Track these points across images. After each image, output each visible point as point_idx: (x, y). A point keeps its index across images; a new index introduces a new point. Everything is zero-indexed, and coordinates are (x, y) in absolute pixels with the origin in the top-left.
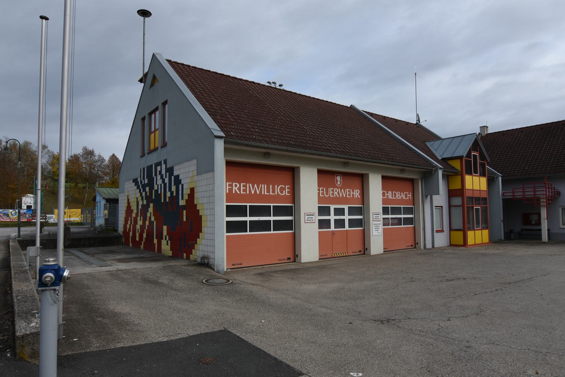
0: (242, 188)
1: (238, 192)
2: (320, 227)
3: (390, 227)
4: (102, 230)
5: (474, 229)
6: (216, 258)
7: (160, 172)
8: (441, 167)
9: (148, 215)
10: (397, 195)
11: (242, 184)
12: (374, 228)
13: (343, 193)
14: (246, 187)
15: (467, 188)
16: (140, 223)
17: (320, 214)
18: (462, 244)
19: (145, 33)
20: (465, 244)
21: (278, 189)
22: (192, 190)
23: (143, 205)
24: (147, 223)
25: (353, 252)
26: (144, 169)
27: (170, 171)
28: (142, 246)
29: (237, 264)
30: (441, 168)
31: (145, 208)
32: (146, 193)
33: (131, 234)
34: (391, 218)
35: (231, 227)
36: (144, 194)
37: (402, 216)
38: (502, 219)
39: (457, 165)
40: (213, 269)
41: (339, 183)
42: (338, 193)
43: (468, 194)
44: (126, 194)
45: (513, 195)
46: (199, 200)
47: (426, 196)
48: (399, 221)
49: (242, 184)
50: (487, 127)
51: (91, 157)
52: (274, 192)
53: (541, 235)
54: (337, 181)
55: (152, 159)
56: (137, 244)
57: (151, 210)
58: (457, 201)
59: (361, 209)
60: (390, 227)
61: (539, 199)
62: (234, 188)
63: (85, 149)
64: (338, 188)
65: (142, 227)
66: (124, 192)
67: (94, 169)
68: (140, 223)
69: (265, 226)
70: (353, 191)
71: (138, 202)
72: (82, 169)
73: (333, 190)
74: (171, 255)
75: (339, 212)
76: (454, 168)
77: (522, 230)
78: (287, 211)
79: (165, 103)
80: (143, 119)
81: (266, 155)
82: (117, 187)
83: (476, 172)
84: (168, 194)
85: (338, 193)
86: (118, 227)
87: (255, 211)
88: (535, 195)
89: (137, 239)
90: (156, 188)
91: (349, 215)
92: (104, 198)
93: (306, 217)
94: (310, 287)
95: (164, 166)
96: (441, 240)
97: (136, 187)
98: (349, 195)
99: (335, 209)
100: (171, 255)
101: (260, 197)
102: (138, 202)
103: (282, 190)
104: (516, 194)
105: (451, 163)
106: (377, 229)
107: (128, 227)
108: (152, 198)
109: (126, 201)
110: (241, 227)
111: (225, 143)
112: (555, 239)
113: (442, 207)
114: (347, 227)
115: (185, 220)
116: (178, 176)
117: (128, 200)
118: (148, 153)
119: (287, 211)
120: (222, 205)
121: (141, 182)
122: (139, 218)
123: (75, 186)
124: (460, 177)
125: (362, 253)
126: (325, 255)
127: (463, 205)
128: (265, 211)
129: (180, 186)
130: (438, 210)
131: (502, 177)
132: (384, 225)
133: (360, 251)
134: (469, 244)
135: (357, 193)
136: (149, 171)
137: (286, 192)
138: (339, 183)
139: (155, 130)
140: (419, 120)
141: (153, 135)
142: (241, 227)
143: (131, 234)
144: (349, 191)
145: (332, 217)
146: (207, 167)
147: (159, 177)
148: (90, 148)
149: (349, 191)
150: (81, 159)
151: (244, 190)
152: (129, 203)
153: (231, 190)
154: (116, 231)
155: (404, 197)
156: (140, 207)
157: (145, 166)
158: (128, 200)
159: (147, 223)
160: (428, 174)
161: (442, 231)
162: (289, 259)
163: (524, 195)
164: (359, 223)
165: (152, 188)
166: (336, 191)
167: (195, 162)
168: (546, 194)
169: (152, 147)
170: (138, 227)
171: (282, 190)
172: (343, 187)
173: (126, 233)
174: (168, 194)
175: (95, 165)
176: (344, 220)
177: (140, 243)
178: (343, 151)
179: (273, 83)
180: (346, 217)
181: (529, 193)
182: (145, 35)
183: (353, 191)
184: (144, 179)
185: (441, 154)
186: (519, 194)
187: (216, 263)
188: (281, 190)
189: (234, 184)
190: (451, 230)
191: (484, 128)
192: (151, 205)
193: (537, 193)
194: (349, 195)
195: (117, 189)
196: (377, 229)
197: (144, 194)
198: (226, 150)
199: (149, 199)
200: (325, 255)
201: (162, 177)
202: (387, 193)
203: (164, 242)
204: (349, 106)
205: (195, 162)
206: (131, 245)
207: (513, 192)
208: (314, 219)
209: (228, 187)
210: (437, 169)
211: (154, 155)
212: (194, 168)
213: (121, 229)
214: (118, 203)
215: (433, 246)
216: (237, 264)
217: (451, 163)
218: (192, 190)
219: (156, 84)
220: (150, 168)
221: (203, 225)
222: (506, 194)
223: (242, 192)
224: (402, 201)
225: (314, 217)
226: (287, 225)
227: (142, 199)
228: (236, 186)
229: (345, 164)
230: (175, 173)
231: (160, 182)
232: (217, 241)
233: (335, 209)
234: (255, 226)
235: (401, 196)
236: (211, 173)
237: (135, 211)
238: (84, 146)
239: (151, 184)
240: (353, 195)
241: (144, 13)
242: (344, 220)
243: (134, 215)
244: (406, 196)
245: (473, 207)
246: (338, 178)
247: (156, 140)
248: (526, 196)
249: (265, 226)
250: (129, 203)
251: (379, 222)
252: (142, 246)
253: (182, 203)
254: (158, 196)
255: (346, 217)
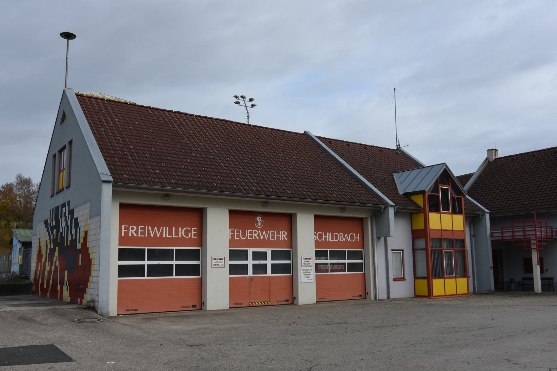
0: (140, 231)
1: (135, 235)
2: (231, 273)
3: (329, 273)
4: (15, 277)
5: (443, 277)
6: (100, 300)
7: (65, 213)
8: (393, 204)
9: (54, 260)
10: (339, 237)
11: (140, 227)
12: (303, 274)
13: (264, 235)
14: (145, 230)
15: (431, 227)
16: (48, 268)
17: (230, 259)
18: (427, 294)
19: (69, 58)
20: (430, 294)
21: (182, 232)
22: (86, 233)
23: (51, 249)
24: (53, 267)
25: (278, 302)
26: (53, 209)
27: (72, 212)
28: (48, 294)
29: (132, 310)
30: (391, 206)
31: (52, 251)
32: (54, 235)
33: (40, 282)
34: (331, 264)
35: (123, 271)
36: (52, 238)
37: (347, 261)
38: (491, 265)
39: (419, 200)
40: (97, 312)
41: (259, 224)
42: (259, 235)
43: (431, 235)
44: (38, 237)
45: (502, 236)
46: (90, 244)
47: (379, 238)
48: (335, 268)
49: (140, 227)
50: (496, 150)
51: (28, 188)
52: (177, 234)
53: (533, 285)
54: (257, 222)
55: (59, 200)
56: (44, 292)
57: (56, 254)
58: (421, 243)
59: (287, 253)
60: (329, 273)
61: (529, 241)
62: (130, 231)
63: (19, 177)
64: (258, 229)
65: (50, 272)
66: (36, 235)
67: (31, 203)
68: (48, 268)
69: (167, 271)
70: (278, 233)
71: (47, 246)
72: (15, 203)
73: (251, 232)
74: (69, 301)
75: (257, 256)
76: (416, 204)
77: (524, 279)
78: (195, 255)
79: (71, 142)
80: (54, 156)
81: (167, 196)
82: (31, 228)
83: (446, 208)
84: (70, 238)
85: (259, 235)
86: (30, 273)
87: (153, 255)
88: (525, 235)
89: (45, 287)
90: (61, 231)
91: (272, 259)
92: (19, 241)
93: (303, 260)
94: (65, 307)
95: (67, 207)
96: (400, 290)
97: (46, 229)
98: (273, 237)
99: (254, 253)
100: (69, 301)
101: (161, 240)
102: (47, 246)
103: (187, 232)
104: (505, 235)
105: (414, 198)
106: (307, 275)
107: (38, 273)
108: (58, 242)
109: (38, 245)
110: (138, 271)
111: (113, 186)
112: (549, 287)
113: (402, 250)
114: (269, 273)
115: (80, 264)
116: (76, 219)
117: (40, 243)
118: (57, 193)
119: (195, 255)
120: (115, 248)
121: (50, 223)
122: (47, 263)
123: (6, 225)
124: (423, 214)
125: (290, 302)
126: (240, 304)
127: (426, 249)
128: (167, 254)
129: (78, 228)
130: (398, 255)
131: (490, 214)
132: (317, 270)
133: (287, 301)
134: (434, 294)
135: (283, 235)
136: (56, 212)
137: (193, 235)
138: (259, 224)
139: (64, 169)
140: (399, 145)
141: (61, 174)
142: (138, 271)
143: (40, 282)
144: (272, 233)
145: (250, 262)
146: (96, 212)
147: (64, 219)
148: (26, 176)
149: (273, 233)
150: (15, 190)
151: (142, 233)
152: (40, 247)
153: (127, 233)
154: (28, 278)
155: (349, 239)
156: (48, 252)
157: (54, 207)
158: (40, 243)
159: (53, 267)
160: (378, 213)
161: (403, 279)
162: (194, 306)
163: (513, 236)
164: (286, 269)
165: (58, 231)
166: (256, 233)
167: (88, 205)
168: (536, 235)
169: (61, 188)
170: (46, 273)
171: (187, 232)
172: (265, 228)
173: (36, 280)
174: (70, 238)
175: (32, 198)
176: (266, 265)
177: (46, 290)
178: (257, 190)
179: (242, 97)
180: (269, 262)
181: (519, 234)
182: (69, 60)
183: (278, 233)
184: (52, 221)
185: (404, 188)
186: (508, 235)
187: (99, 306)
188: (185, 233)
189: (130, 227)
190: (415, 278)
191: (492, 151)
192: (57, 248)
193: (527, 233)
194: (273, 237)
195: (31, 231)
196: (307, 275)
197: (52, 238)
198: (115, 194)
199: (55, 241)
200: (240, 304)
201: (66, 220)
202: (325, 235)
203: (65, 288)
204: (303, 132)
205: (88, 205)
206: (40, 293)
207: (502, 233)
208: (311, 262)
209: (123, 230)
210: (387, 205)
211: (61, 195)
212: (88, 211)
213: (32, 277)
214: (31, 247)
215: (388, 297)
216: (132, 310)
217: (414, 198)
218: (86, 233)
219: (65, 121)
220: (57, 208)
221: (92, 269)
222: (494, 235)
223: (139, 235)
224: (346, 244)
225: (310, 260)
226: (195, 270)
227: (50, 243)
228: (133, 229)
229: (265, 204)
230: (75, 217)
231: (64, 224)
232: (107, 285)
233: (254, 253)
234: (154, 271)
235: (344, 238)
236: (98, 217)
237: (44, 256)
238: (19, 174)
239: (57, 227)
240: (278, 237)
241: (68, 36)
242: (266, 265)
243: (43, 260)
244: (352, 237)
245: (442, 251)
246: (259, 219)
247: (63, 181)
248: (516, 237)
249: (167, 271)
250: (40, 247)
251: (311, 268)
252: (48, 294)
253: (79, 246)
254: (62, 238)
255: (269, 262)
